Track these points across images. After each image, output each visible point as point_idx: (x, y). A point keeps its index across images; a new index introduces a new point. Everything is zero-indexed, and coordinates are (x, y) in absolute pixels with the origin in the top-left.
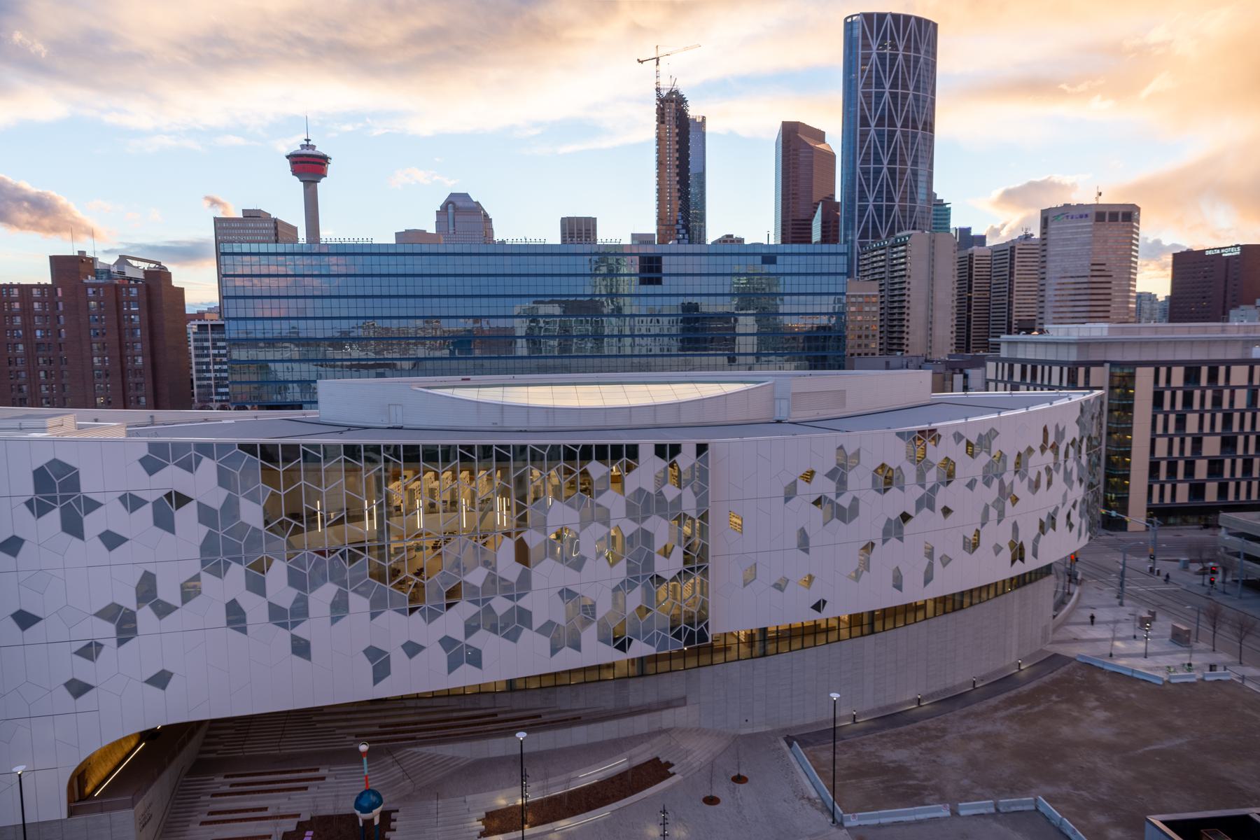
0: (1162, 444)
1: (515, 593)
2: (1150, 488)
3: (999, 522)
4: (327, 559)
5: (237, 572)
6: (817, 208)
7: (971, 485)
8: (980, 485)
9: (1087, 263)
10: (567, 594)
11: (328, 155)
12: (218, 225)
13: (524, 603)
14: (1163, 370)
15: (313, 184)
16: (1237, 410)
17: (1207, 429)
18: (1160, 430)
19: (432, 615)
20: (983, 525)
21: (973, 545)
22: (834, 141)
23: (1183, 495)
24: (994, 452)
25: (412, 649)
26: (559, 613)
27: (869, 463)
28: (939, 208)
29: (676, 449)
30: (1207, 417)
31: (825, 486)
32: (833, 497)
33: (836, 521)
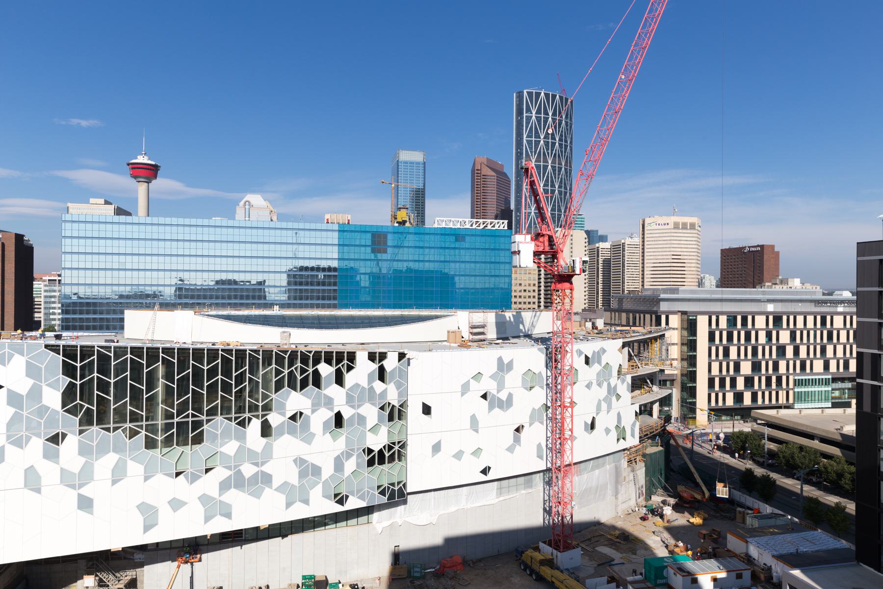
0: (715, 366)
1: (260, 461)
2: (709, 396)
3: (608, 412)
4: (112, 434)
5: (37, 444)
8: (595, 386)
10: (300, 462)
13: (266, 468)
14: (714, 318)
16: (760, 345)
17: (742, 356)
18: (713, 357)
19: (194, 478)
20: (597, 414)
24: (603, 364)
25: (176, 504)
26: (292, 476)
29: (383, 356)
30: (742, 349)
32: (494, 392)
33: (497, 410)
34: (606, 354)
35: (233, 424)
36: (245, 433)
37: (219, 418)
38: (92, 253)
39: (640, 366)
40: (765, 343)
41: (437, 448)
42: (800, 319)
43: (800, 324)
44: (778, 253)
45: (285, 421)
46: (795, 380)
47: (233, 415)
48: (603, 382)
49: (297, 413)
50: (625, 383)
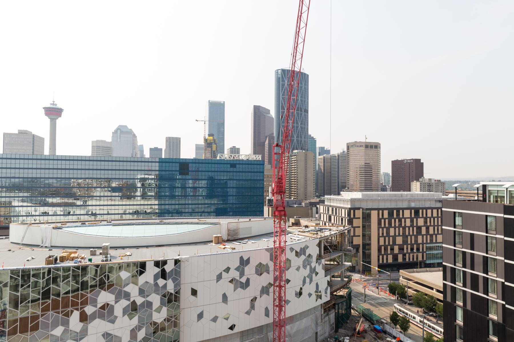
0: (382, 240)
2: (379, 257)
3: (310, 283)
6: (267, 138)
7: (298, 269)
8: (302, 268)
9: (363, 164)
11: (63, 109)
12: (5, 136)
14: (381, 212)
15: (55, 120)
18: (381, 235)
20: (303, 286)
21: (300, 294)
22: (273, 113)
23: (390, 260)
24: (307, 255)
27: (254, 263)
28: (312, 140)
31: (234, 274)
32: (238, 278)
33: (239, 289)
34: (308, 249)
35: (60, 315)
36: (68, 321)
37: (51, 312)
38: (24, 159)
39: (331, 251)
40: (409, 225)
41: (200, 316)
42: (429, 211)
43: (429, 215)
44: (423, 163)
45: (96, 310)
46: (426, 247)
47: (60, 310)
48: (307, 266)
49: (105, 304)
50: (321, 265)
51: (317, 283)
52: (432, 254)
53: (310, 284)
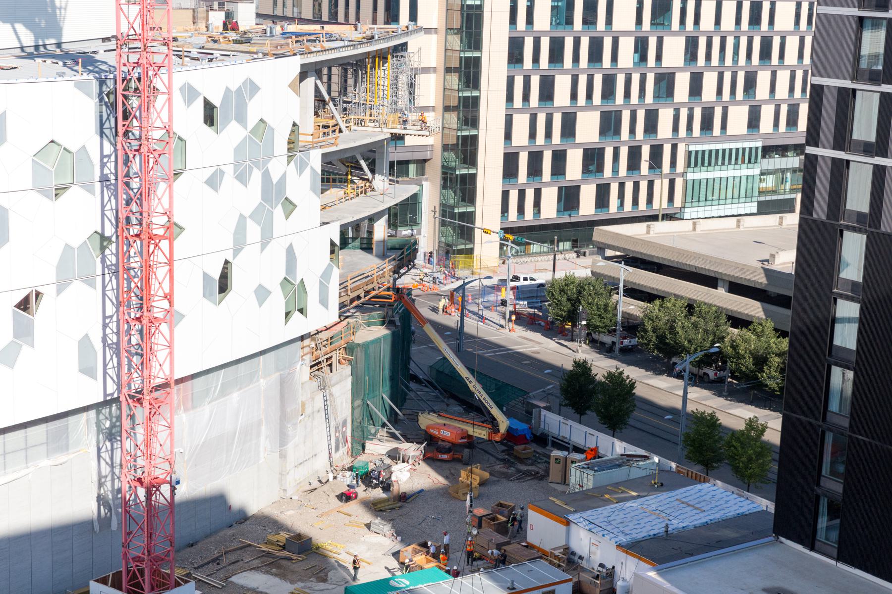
8: (229, 180)
24: (252, 122)
48: (251, 169)
51: (291, 246)
52: (704, 183)
53: (262, 250)
